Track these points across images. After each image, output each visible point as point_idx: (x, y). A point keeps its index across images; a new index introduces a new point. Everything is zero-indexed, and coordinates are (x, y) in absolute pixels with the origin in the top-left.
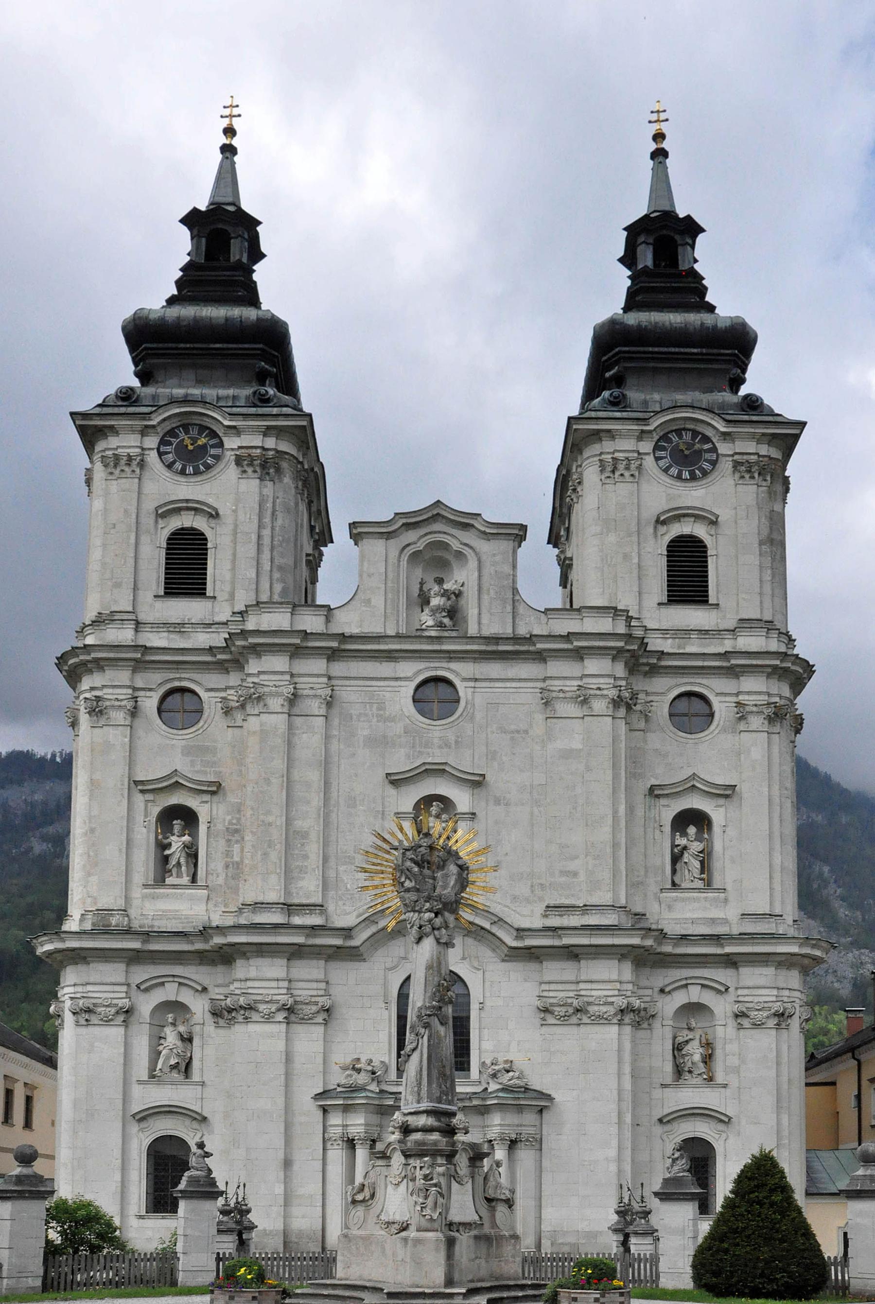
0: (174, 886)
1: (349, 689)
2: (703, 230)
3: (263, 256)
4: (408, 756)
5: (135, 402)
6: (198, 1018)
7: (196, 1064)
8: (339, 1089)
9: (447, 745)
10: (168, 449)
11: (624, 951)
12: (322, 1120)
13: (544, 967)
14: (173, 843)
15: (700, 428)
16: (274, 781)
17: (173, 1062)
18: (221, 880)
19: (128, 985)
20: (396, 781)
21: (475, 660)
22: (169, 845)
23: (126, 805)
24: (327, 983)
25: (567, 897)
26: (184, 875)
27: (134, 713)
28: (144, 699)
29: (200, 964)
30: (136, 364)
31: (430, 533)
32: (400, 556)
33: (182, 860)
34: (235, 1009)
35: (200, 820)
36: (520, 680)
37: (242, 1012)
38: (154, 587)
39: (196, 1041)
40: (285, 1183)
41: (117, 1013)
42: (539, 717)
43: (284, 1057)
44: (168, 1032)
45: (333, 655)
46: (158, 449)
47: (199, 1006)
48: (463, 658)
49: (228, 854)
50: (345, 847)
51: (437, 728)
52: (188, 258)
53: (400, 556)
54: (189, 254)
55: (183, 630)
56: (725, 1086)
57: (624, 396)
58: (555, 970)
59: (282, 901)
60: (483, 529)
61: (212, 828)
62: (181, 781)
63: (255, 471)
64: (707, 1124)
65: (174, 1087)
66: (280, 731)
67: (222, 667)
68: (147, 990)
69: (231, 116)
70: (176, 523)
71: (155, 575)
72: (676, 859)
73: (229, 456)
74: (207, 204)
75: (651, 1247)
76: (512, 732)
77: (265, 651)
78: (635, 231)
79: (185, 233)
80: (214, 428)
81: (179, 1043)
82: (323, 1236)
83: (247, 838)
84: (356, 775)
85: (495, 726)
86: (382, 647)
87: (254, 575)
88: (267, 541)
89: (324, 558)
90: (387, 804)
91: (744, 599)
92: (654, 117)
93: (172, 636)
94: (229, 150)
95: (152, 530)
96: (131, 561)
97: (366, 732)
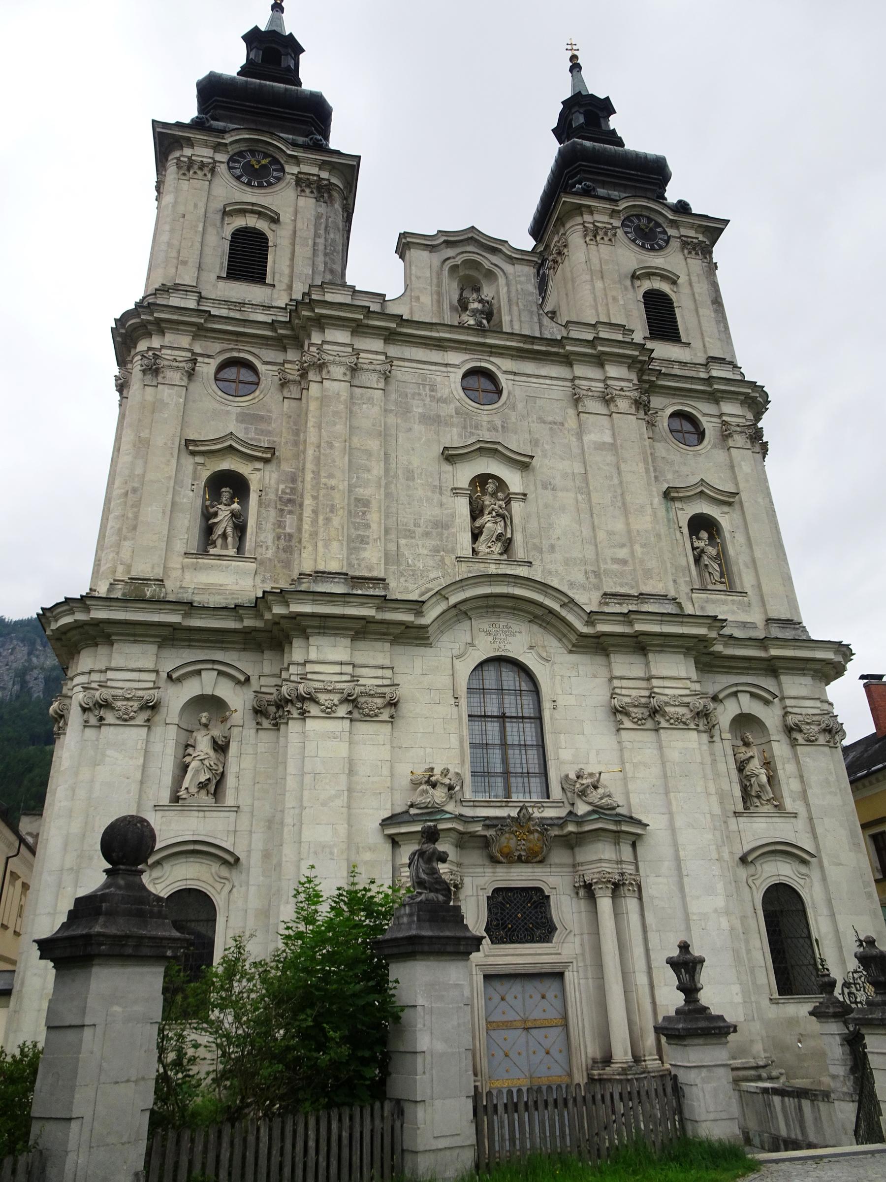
0: (219, 557)
1: (403, 369)
4: (460, 436)
6: (236, 718)
7: (230, 781)
8: (413, 811)
9: (495, 429)
10: (237, 165)
11: (690, 643)
12: (390, 858)
13: (613, 660)
14: (220, 512)
15: (653, 216)
16: (337, 445)
17: (203, 778)
18: (269, 554)
20: (450, 457)
21: (512, 357)
22: (216, 514)
23: (175, 465)
25: (622, 585)
26: (230, 547)
27: (191, 374)
28: (202, 365)
29: (244, 649)
31: (466, 252)
32: (442, 266)
33: (229, 531)
34: (291, 701)
35: (252, 488)
36: (552, 378)
37: (299, 705)
38: (217, 270)
39: (233, 748)
41: (141, 708)
42: (571, 412)
43: (347, 765)
44: (199, 738)
45: (390, 337)
47: (239, 701)
48: (502, 354)
49: (280, 524)
50: (405, 520)
51: (485, 412)
53: (442, 266)
56: (795, 815)
58: (626, 666)
59: (344, 571)
61: (263, 497)
63: (312, 192)
64: (788, 865)
65: (201, 814)
66: (342, 398)
67: (280, 344)
68: (179, 680)
70: (240, 222)
71: (218, 261)
76: (550, 423)
77: (328, 324)
80: (277, 156)
81: (212, 753)
84: (413, 449)
85: (535, 417)
86: (435, 334)
88: (321, 247)
90: (444, 480)
92: (569, 47)
95: (218, 223)
96: (198, 246)
97: (420, 410)
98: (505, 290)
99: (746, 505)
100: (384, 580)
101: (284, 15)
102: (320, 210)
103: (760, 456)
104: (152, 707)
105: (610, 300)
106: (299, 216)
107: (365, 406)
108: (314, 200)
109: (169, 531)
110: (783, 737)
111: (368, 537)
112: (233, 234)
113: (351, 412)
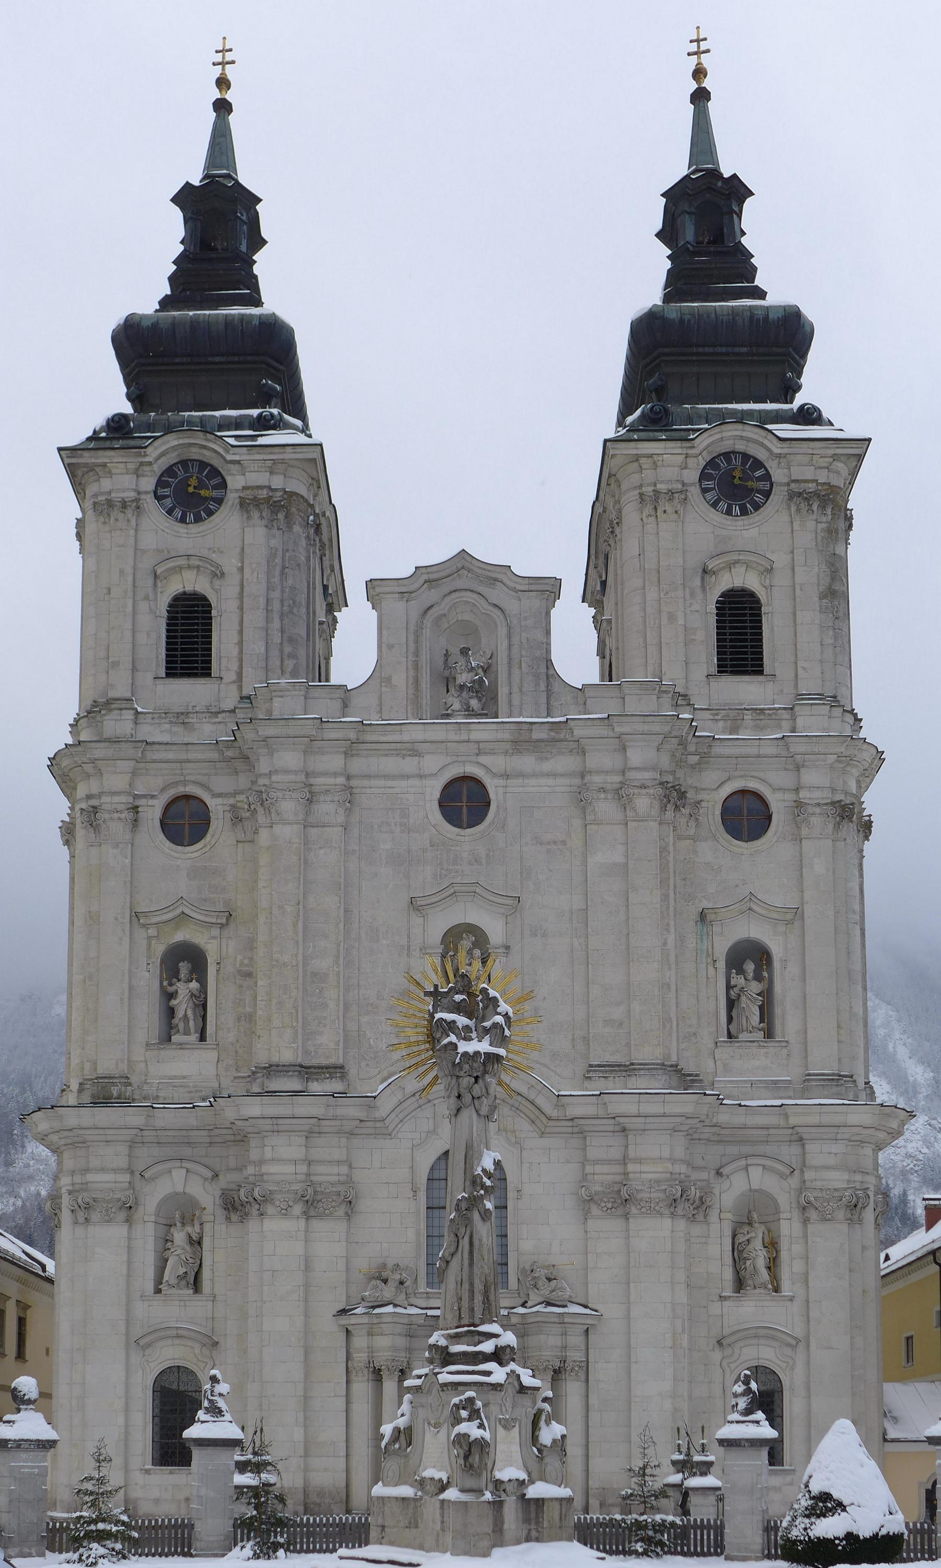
2: (752, 194)
3: (264, 242)
5: (126, 433)
7: (206, 1274)
12: (344, 1344)
14: (180, 992)
16: (289, 909)
17: (181, 1271)
19: (132, 1173)
24: (350, 1166)
30: (128, 385)
33: (190, 1013)
40: (306, 1427)
46: (155, 492)
52: (182, 248)
54: (182, 242)
55: (186, 721)
57: (666, 411)
59: (299, 1061)
60: (513, 585)
62: (187, 911)
69: (223, 64)
72: (731, 1004)
73: (232, 498)
74: (201, 177)
75: (713, 1510)
76: (549, 843)
78: (675, 197)
79: (176, 216)
81: (188, 1248)
82: (348, 1496)
83: (260, 983)
87: (263, 650)
88: (276, 605)
89: (338, 626)
91: (804, 668)
93: (175, 729)
94: (222, 107)
96: (128, 635)
97: (388, 846)
98: (505, 644)
99: (808, 921)
100: (342, 1067)
101: (231, 118)
102: (274, 543)
103: (861, 835)
104: (129, 1208)
105: (664, 621)
106: (246, 562)
107: (322, 851)
108: (264, 529)
109: (129, 1022)
110: (796, 1214)
111: (325, 1018)
112: (170, 606)
113: (306, 862)
